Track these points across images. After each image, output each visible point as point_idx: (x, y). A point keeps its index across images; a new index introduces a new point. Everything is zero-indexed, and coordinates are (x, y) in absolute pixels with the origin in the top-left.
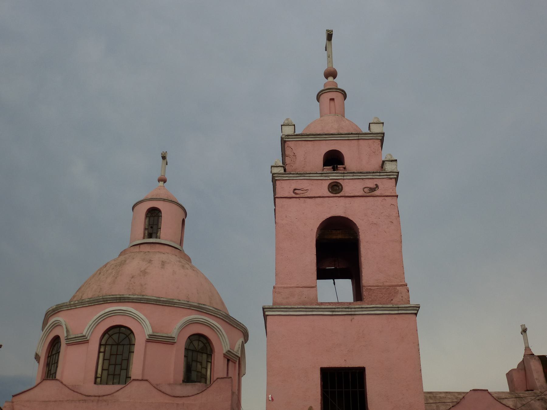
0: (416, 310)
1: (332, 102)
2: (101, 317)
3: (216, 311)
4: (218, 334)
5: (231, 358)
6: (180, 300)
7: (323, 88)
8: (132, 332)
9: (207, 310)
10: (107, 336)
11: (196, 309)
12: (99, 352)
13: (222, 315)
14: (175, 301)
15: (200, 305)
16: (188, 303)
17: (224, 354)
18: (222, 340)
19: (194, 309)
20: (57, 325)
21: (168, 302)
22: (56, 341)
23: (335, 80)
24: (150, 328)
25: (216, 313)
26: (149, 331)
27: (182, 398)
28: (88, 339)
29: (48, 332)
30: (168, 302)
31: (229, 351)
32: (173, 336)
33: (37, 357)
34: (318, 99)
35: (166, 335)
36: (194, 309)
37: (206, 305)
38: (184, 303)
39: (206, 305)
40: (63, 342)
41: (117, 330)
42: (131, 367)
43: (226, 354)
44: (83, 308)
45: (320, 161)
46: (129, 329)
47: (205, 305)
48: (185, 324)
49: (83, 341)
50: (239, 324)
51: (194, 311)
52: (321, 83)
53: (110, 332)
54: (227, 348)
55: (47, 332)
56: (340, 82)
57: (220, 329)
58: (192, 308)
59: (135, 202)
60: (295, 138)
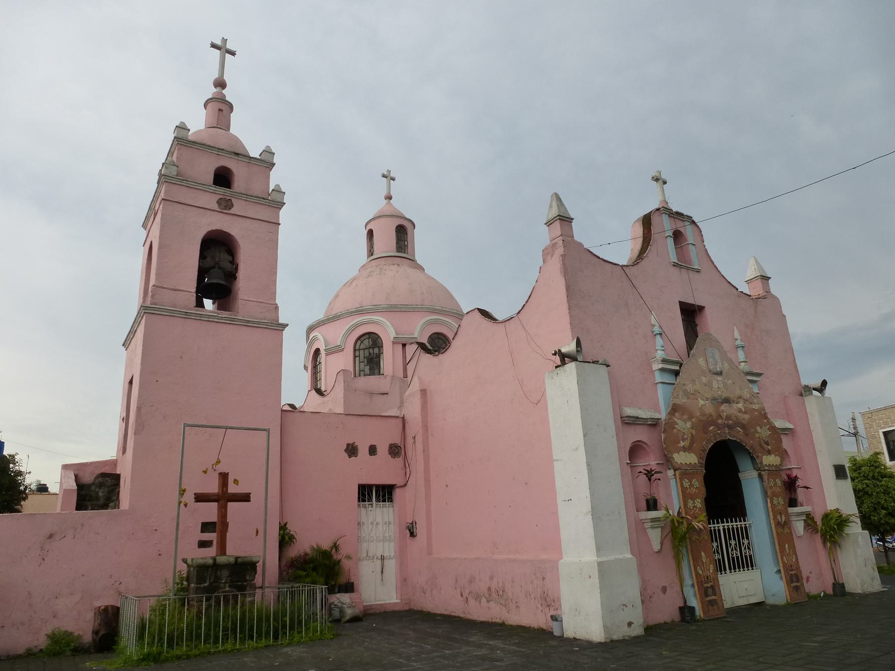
0: (283, 328)
1: (221, 112)
6: (341, 312)
7: (211, 97)
8: (379, 336)
12: (355, 357)
14: (338, 314)
17: (393, 342)
20: (315, 339)
21: (335, 317)
22: (317, 351)
24: (392, 329)
26: (393, 334)
28: (343, 347)
30: (335, 317)
32: (416, 337)
33: (306, 368)
34: (205, 106)
35: (334, 346)
40: (323, 352)
41: (367, 336)
44: (267, 330)
45: (210, 178)
46: (377, 334)
49: (338, 349)
50: (415, 306)
52: (211, 91)
53: (362, 339)
57: (451, 324)
59: (367, 221)
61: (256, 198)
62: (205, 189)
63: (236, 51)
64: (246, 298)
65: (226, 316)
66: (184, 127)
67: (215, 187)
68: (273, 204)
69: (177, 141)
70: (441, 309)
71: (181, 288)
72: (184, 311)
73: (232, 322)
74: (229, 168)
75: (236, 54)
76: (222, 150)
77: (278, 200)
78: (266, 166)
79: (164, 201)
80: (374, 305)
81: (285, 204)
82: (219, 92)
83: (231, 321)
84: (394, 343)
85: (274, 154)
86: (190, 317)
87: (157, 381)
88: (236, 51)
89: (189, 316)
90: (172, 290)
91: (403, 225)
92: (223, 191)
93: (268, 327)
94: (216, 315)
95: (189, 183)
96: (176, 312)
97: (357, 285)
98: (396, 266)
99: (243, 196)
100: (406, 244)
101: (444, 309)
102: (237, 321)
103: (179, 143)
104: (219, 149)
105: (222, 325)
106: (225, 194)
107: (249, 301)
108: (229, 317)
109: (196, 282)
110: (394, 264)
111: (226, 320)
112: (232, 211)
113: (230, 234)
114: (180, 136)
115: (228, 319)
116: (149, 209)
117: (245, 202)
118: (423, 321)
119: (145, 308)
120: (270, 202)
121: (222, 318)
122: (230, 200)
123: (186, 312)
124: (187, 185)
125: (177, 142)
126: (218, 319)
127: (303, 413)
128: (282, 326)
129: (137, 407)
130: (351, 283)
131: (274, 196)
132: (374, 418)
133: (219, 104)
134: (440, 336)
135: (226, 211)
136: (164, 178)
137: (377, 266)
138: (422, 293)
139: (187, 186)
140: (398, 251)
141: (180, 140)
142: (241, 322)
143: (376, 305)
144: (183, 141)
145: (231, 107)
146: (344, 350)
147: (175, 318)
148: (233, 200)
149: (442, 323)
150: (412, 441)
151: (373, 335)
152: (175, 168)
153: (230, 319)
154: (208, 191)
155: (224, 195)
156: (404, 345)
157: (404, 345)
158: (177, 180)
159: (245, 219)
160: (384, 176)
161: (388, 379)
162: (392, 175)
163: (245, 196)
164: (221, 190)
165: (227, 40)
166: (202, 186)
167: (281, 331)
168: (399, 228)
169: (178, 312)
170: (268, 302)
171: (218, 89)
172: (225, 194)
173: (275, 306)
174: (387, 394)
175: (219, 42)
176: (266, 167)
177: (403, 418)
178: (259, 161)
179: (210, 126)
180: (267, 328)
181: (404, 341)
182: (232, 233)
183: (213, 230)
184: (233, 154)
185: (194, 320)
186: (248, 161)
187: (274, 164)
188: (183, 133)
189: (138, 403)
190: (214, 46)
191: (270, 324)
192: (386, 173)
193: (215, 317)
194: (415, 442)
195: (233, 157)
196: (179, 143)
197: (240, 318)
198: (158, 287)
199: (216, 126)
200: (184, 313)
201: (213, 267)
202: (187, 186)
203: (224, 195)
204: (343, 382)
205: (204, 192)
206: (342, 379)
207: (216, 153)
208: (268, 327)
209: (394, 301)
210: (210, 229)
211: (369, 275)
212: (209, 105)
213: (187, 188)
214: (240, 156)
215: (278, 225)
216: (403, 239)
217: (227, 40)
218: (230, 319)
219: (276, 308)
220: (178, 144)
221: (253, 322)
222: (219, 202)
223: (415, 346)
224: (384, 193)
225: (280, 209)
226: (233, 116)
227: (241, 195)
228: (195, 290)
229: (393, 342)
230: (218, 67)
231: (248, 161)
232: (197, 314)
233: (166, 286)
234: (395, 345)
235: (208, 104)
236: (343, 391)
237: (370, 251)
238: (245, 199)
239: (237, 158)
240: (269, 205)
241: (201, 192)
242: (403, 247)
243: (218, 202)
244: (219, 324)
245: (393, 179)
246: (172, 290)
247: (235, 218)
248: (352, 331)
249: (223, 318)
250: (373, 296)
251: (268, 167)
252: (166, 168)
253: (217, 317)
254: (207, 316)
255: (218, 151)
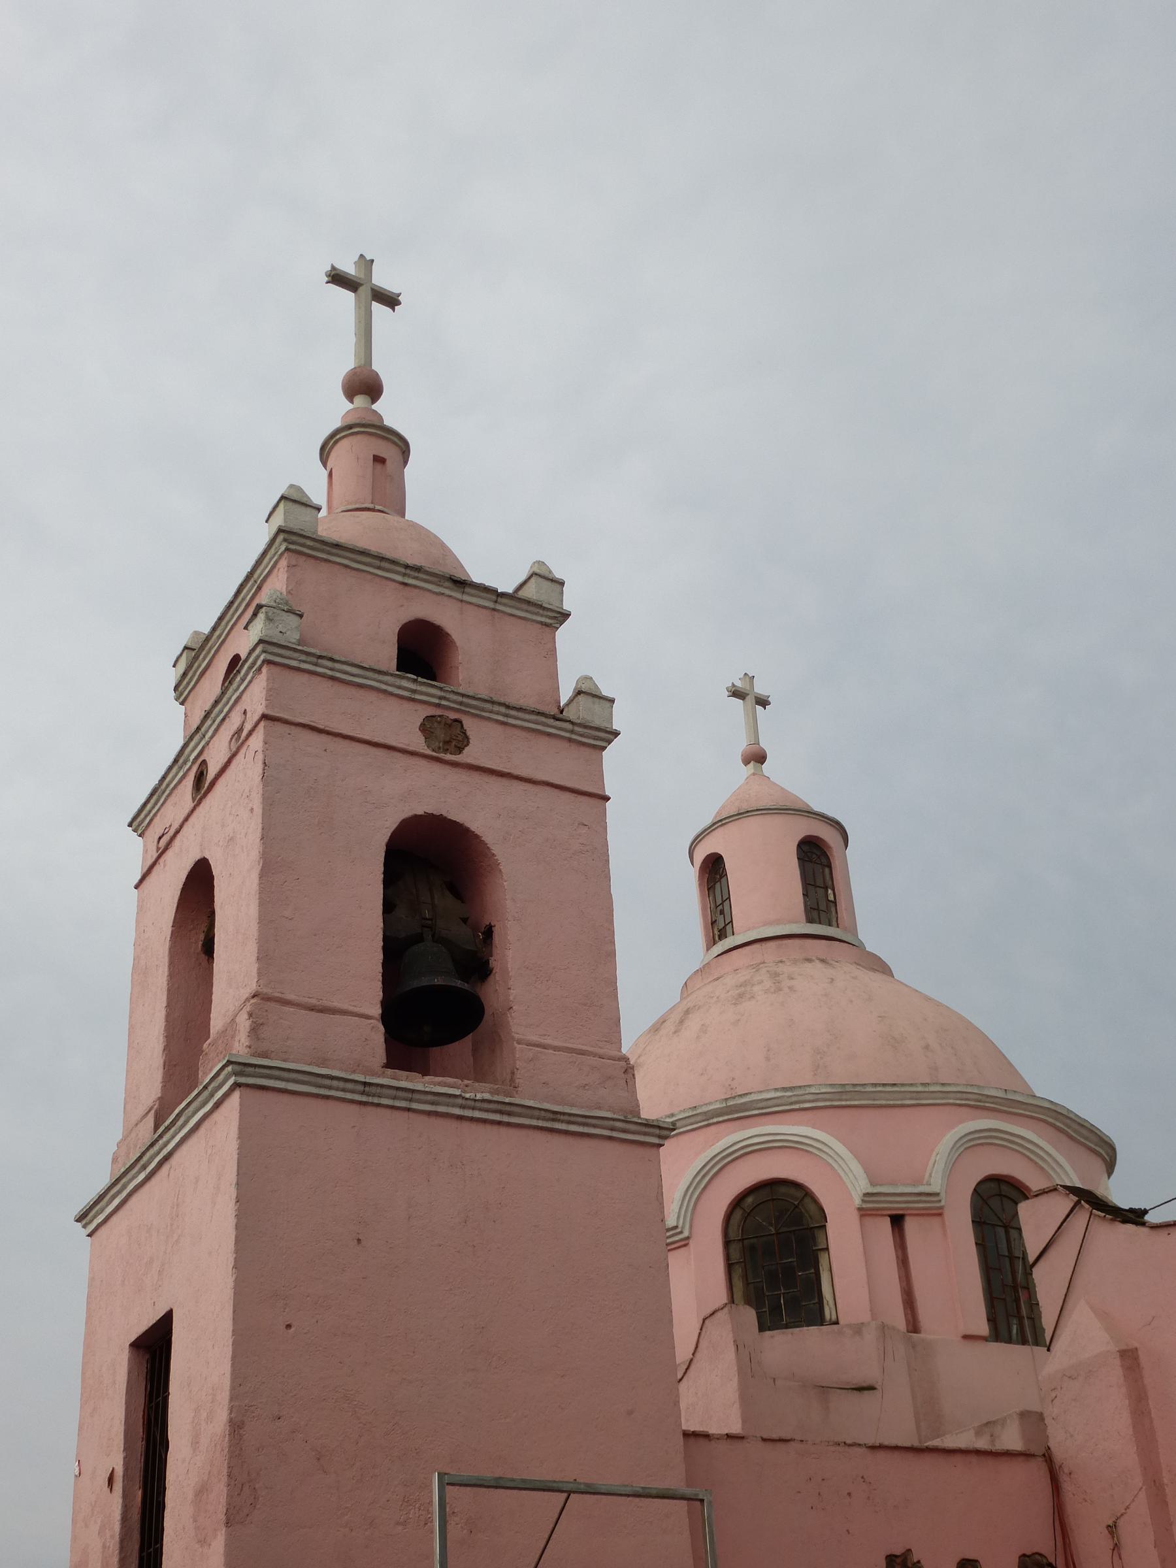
0: (660, 1137)
1: (379, 466)
2: (713, 1162)
3: (791, 1096)
4: (824, 1156)
5: (908, 1209)
7: (337, 424)
9: (760, 1105)
10: (738, 1214)
11: (726, 1118)
13: (820, 1096)
15: (731, 1103)
16: (695, 1113)
17: (860, 1209)
18: (840, 1171)
19: (721, 1119)
23: (374, 407)
24: (856, 1167)
25: (794, 1099)
26: (858, 1184)
27: (1062, 1314)
28: (686, 1234)
29: (979, 1138)
31: (867, 1195)
36: (721, 1119)
37: (751, 1093)
38: (685, 1118)
39: (751, 1093)
42: (728, 1296)
43: (864, 1206)
45: (387, 655)
47: (747, 1094)
48: (704, 1176)
50: (920, 1089)
51: (723, 1125)
54: (858, 1189)
55: (979, 1138)
56: (388, 410)
58: (715, 1120)
60: (173, 1137)
61: (533, 717)
62: (384, 687)
63: (399, 295)
64: (534, 1038)
65: (487, 1096)
66: (304, 500)
67: (415, 681)
68: (581, 735)
69: (285, 540)
70: (1001, 1094)
71: (336, 1004)
72: (361, 1078)
73: (506, 1119)
74: (439, 626)
75: (399, 303)
76: (418, 569)
77: (597, 722)
78: (543, 619)
79: (269, 723)
80: (784, 1089)
81: (616, 734)
82: (366, 408)
83: (501, 1112)
84: (863, 1213)
85: (562, 584)
86: (376, 1100)
87: (289, 1326)
88: (399, 295)
89: (374, 1095)
90: (312, 1009)
91: (817, 838)
92: (439, 693)
93: (615, 1134)
94: (457, 1092)
95: (338, 666)
96: (335, 1083)
97: (704, 1029)
98: (818, 964)
99: (496, 708)
100: (831, 898)
101: (1010, 1096)
102: (520, 1115)
103: (292, 547)
104: (407, 567)
105: (474, 1127)
106: (444, 702)
107: (545, 1047)
108: (496, 1098)
109: (380, 985)
110: (809, 960)
111: (487, 1111)
112: (468, 756)
113: (467, 830)
114: (294, 526)
115: (492, 1106)
116: (176, 761)
117: (500, 728)
118: (948, 1136)
119: (238, 1068)
120: (577, 729)
121: (474, 1104)
122: (456, 720)
123: (365, 1084)
124: (329, 673)
125: (283, 548)
126: (462, 1107)
127: (702, 1441)
128: (657, 1131)
129: (231, 1421)
130: (682, 1022)
131: (583, 711)
132: (958, 1459)
133: (373, 440)
134: (1004, 1188)
135: (448, 757)
136: (264, 652)
137: (757, 967)
138: (927, 1047)
139: (332, 678)
140: (810, 920)
141: (294, 538)
142: (531, 1117)
143: (791, 1089)
144: (302, 540)
145: (403, 447)
146: (691, 1242)
147: (331, 1103)
148: (468, 723)
149: (1008, 1143)
150: (1107, 1544)
151: (783, 1189)
152: (293, 620)
153: (499, 1107)
154: (391, 694)
155: (438, 706)
156: (897, 1221)
157: (897, 1221)
158: (303, 657)
159: (505, 782)
160: (737, 693)
161: (870, 1336)
162: (760, 689)
163: (503, 710)
164: (427, 690)
165: (372, 261)
166: (376, 676)
167: (654, 1150)
168: (805, 848)
169: (341, 1084)
170: (601, 1051)
171: (360, 401)
172: (444, 702)
173: (623, 1063)
174: (871, 1388)
175: (349, 267)
176: (541, 623)
177: (1048, 1457)
178: (525, 607)
179: (350, 507)
180: (610, 1138)
181: (897, 1207)
182: (475, 826)
183: (416, 816)
184: (447, 584)
185: (388, 1112)
186: (491, 605)
187: (566, 616)
188: (300, 520)
189: (231, 1410)
190: (337, 278)
191: (619, 1124)
192: (739, 684)
193: (451, 1100)
194: (1116, 1547)
195: (447, 592)
196: (292, 547)
197: (531, 1103)
198: (268, 999)
199: (371, 506)
200: (361, 1088)
201: (419, 939)
202: (332, 678)
203: (438, 706)
204: (733, 1349)
205: (382, 696)
206: (729, 1339)
207: (399, 578)
208: (615, 1134)
209: (842, 1074)
210: (407, 813)
211: (741, 996)
212: (343, 452)
213: (330, 683)
214: (467, 590)
215: (601, 802)
216: (820, 882)
217: (372, 261)
218: (499, 1107)
219: (625, 1072)
220: (287, 549)
221: (570, 1118)
222: (427, 727)
223: (1062, 1204)
224: (742, 744)
225: (604, 748)
226: (411, 472)
227: (488, 706)
228: (380, 1011)
229: (860, 1209)
230: (353, 339)
231: (491, 605)
232: (398, 1089)
233: (291, 997)
234: (869, 1221)
235: (336, 442)
236: (736, 1379)
237: (713, 923)
238: (500, 718)
239: (458, 595)
240: (570, 740)
241: (372, 696)
242: (823, 906)
243: (423, 728)
244: (466, 1125)
245: (763, 702)
246: (312, 1009)
247: (476, 777)
248: (712, 1178)
249: (478, 1105)
250: (768, 1059)
251: (547, 625)
252: (269, 619)
253: (460, 1101)
254: (430, 1097)
255: (404, 575)
